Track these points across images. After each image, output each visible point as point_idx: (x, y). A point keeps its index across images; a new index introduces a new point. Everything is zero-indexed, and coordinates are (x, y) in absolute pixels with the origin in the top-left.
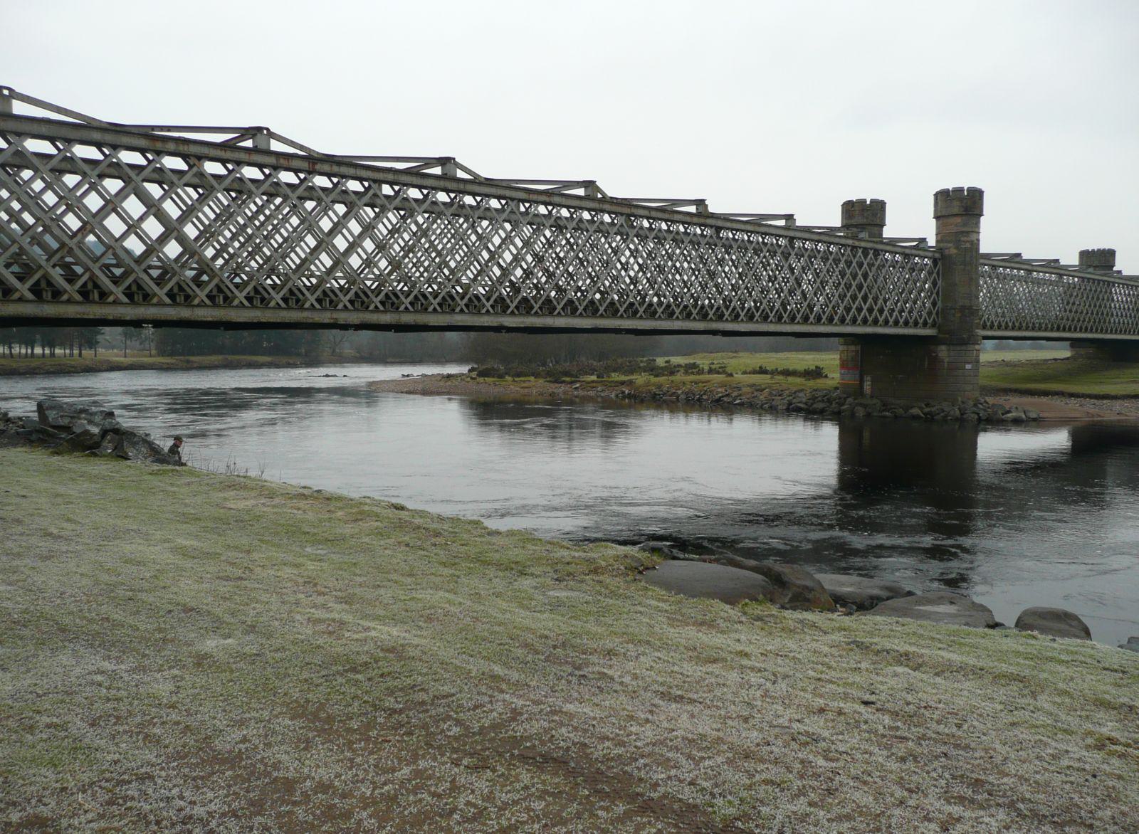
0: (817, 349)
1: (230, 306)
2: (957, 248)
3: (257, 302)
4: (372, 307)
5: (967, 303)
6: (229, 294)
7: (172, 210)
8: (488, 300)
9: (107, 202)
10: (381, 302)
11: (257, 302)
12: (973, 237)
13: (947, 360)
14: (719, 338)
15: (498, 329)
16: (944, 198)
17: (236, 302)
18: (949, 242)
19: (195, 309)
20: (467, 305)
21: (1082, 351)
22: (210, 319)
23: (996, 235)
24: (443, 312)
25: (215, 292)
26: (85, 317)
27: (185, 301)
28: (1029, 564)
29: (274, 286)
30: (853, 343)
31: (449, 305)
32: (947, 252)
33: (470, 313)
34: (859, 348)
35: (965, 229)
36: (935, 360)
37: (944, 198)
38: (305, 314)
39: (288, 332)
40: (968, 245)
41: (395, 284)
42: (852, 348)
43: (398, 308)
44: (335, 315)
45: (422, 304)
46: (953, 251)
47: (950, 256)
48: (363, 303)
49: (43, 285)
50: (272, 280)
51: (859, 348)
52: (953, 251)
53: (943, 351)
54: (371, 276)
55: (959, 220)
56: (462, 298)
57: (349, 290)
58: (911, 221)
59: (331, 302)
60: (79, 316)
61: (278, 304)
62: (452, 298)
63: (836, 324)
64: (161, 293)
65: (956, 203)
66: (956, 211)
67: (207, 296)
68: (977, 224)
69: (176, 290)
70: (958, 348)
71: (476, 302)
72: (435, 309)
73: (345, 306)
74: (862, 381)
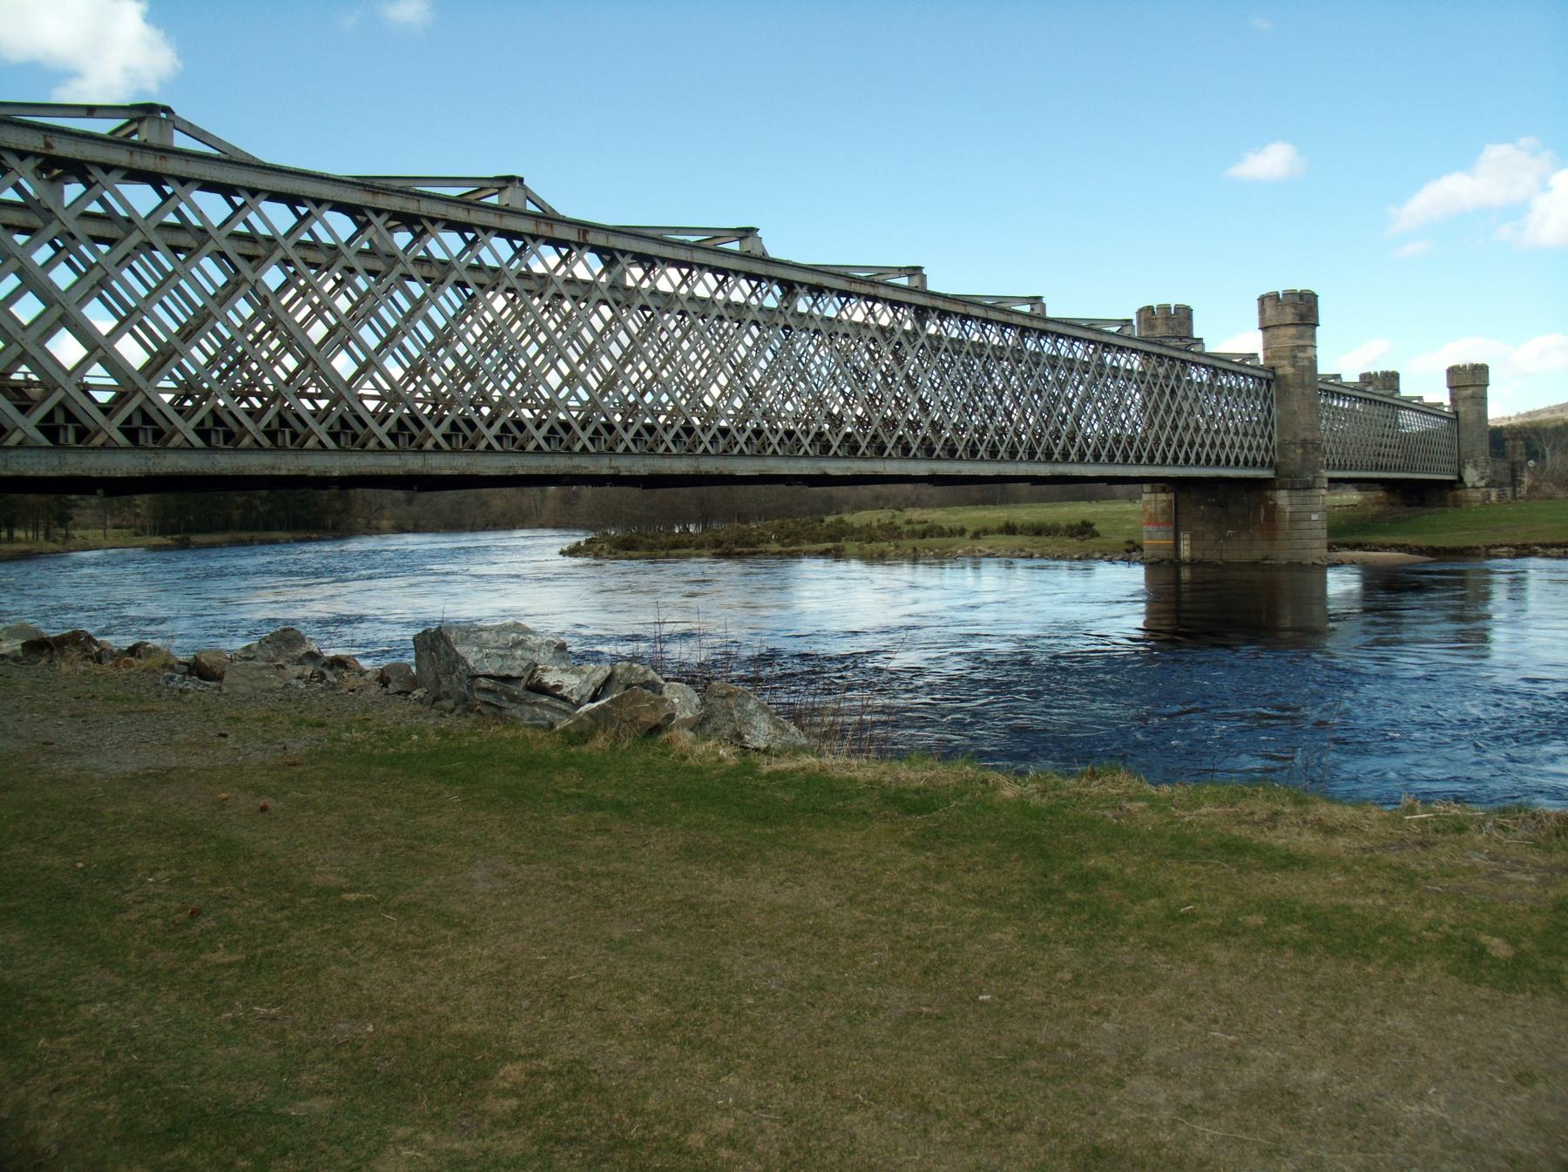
0: (1089, 498)
1: (165, 448)
2: (1293, 366)
3: (145, 438)
4: (372, 444)
5: (1309, 436)
6: (235, 428)
7: (63, 277)
8: (583, 428)
9: (103, 283)
10: (390, 434)
11: (145, 438)
12: (1309, 352)
13: (1288, 509)
14: (908, 487)
15: (617, 480)
16: (1453, 372)
17: (176, 440)
18: (1281, 358)
19: (428, 456)
20: (499, 439)
21: (1371, 495)
22: (448, 472)
23: (1341, 354)
24: (455, 451)
25: (209, 424)
26: (276, 472)
27: (79, 439)
28: (1532, 631)
29: (251, 413)
30: (1164, 491)
31: (515, 439)
32: (1280, 372)
33: (505, 452)
34: (1171, 496)
35: (1301, 342)
36: (1273, 510)
37: (1453, 372)
38: (576, 461)
39: (1012, 485)
40: (1306, 363)
41: (419, 405)
42: (1162, 496)
43: (364, 445)
44: (615, 463)
45: (465, 438)
46: (1289, 370)
47: (1285, 376)
48: (355, 437)
49: (60, 418)
50: (250, 403)
51: (1171, 496)
52: (1289, 370)
53: (1282, 498)
54: (420, 395)
55: (1292, 331)
56: (490, 425)
57: (387, 416)
58: (1231, 332)
59: (294, 436)
60: (267, 472)
61: (320, 442)
62: (471, 424)
63: (1104, 463)
64: (187, 428)
65: (1289, 310)
66: (1289, 319)
67: (196, 431)
68: (1313, 337)
69: (209, 424)
70: (1302, 493)
71: (562, 434)
72: (489, 447)
73: (380, 444)
74: (1177, 540)
